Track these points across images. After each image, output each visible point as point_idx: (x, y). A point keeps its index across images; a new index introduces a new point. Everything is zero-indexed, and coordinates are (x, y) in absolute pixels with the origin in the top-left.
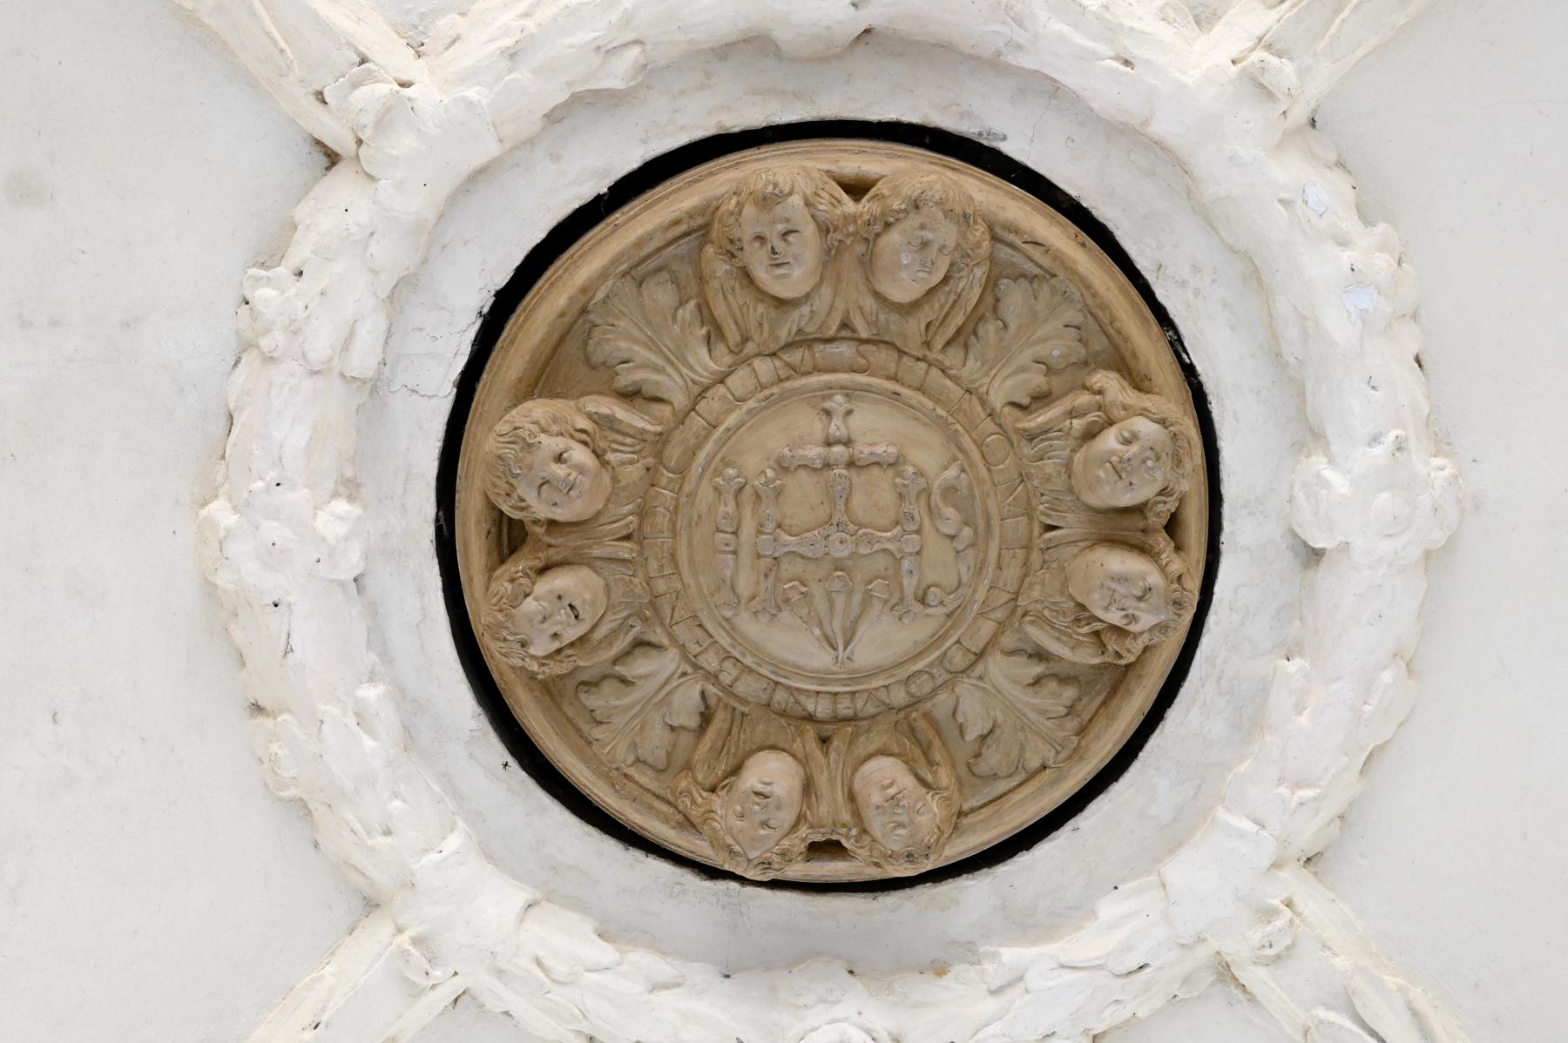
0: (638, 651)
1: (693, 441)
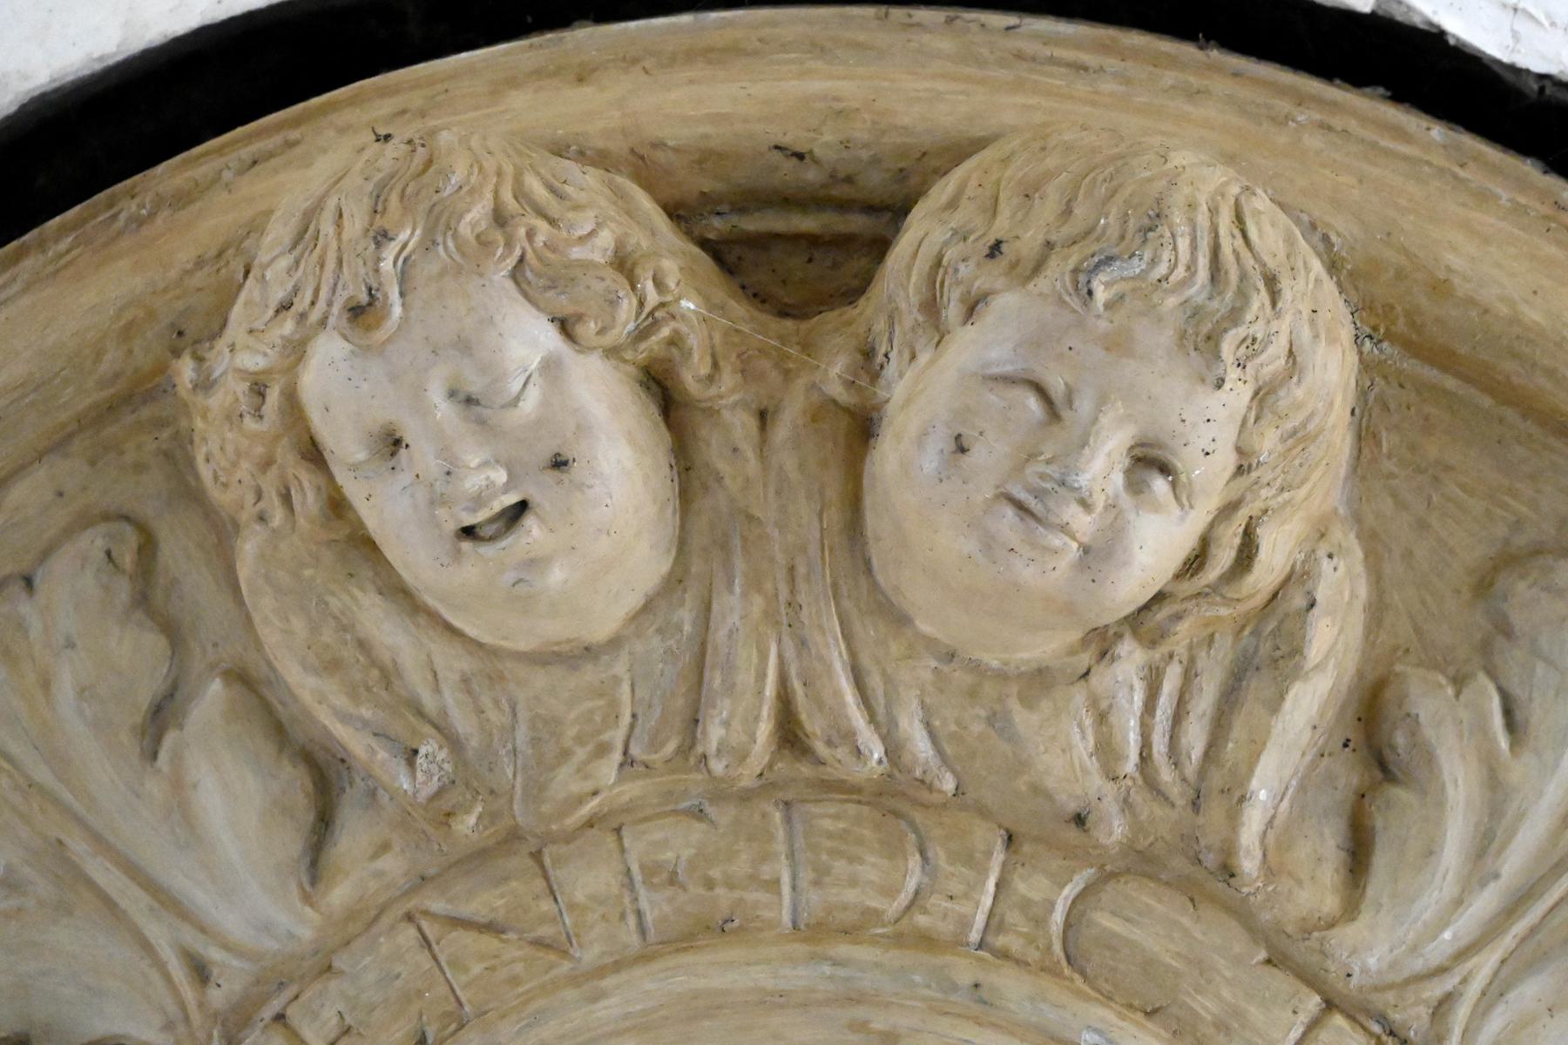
0: (294, 780)
1: (1206, 1006)
